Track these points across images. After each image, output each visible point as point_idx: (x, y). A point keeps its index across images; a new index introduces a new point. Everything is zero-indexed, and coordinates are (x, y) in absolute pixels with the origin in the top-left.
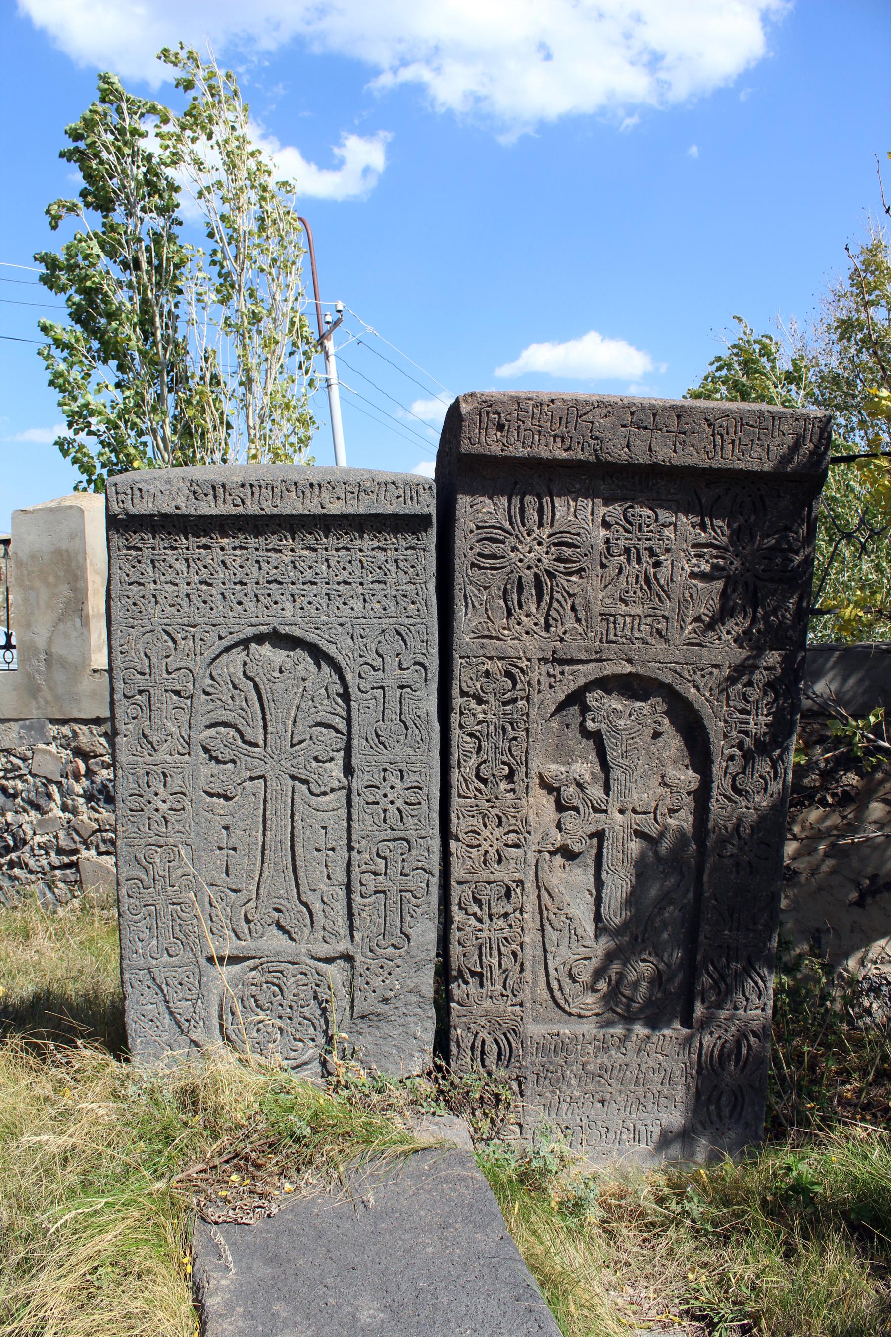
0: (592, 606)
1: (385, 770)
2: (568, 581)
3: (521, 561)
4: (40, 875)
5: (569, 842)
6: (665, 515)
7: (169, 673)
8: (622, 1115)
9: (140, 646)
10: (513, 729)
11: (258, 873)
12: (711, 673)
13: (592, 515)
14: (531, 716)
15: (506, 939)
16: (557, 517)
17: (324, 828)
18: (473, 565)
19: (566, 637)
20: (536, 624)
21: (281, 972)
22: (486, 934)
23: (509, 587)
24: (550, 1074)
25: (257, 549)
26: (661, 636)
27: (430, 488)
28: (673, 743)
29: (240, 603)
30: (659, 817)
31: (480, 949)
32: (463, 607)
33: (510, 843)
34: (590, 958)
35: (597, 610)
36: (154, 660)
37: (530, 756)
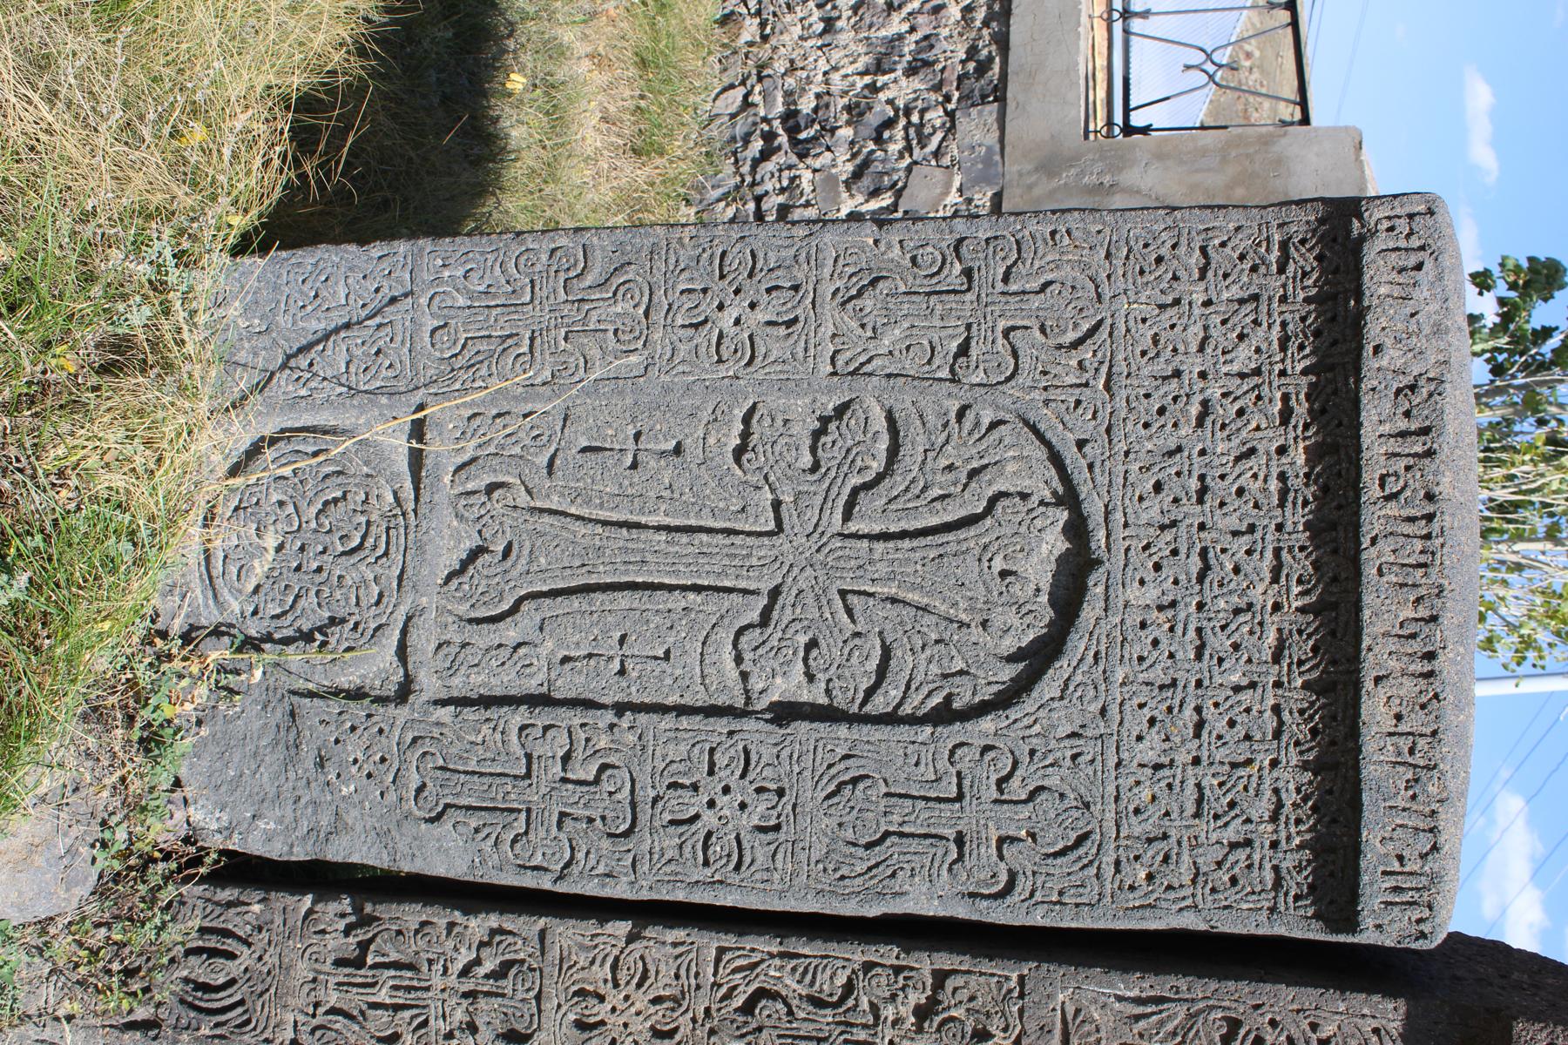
1: (781, 793)
4: (748, 179)
7: (1006, 333)
9: (1067, 273)
11: (585, 512)
15: (425, 1023)
21: (386, 554)
22: (437, 981)
25: (1279, 527)
27: (1423, 935)
29: (1158, 487)
31: (410, 967)
36: (1036, 302)
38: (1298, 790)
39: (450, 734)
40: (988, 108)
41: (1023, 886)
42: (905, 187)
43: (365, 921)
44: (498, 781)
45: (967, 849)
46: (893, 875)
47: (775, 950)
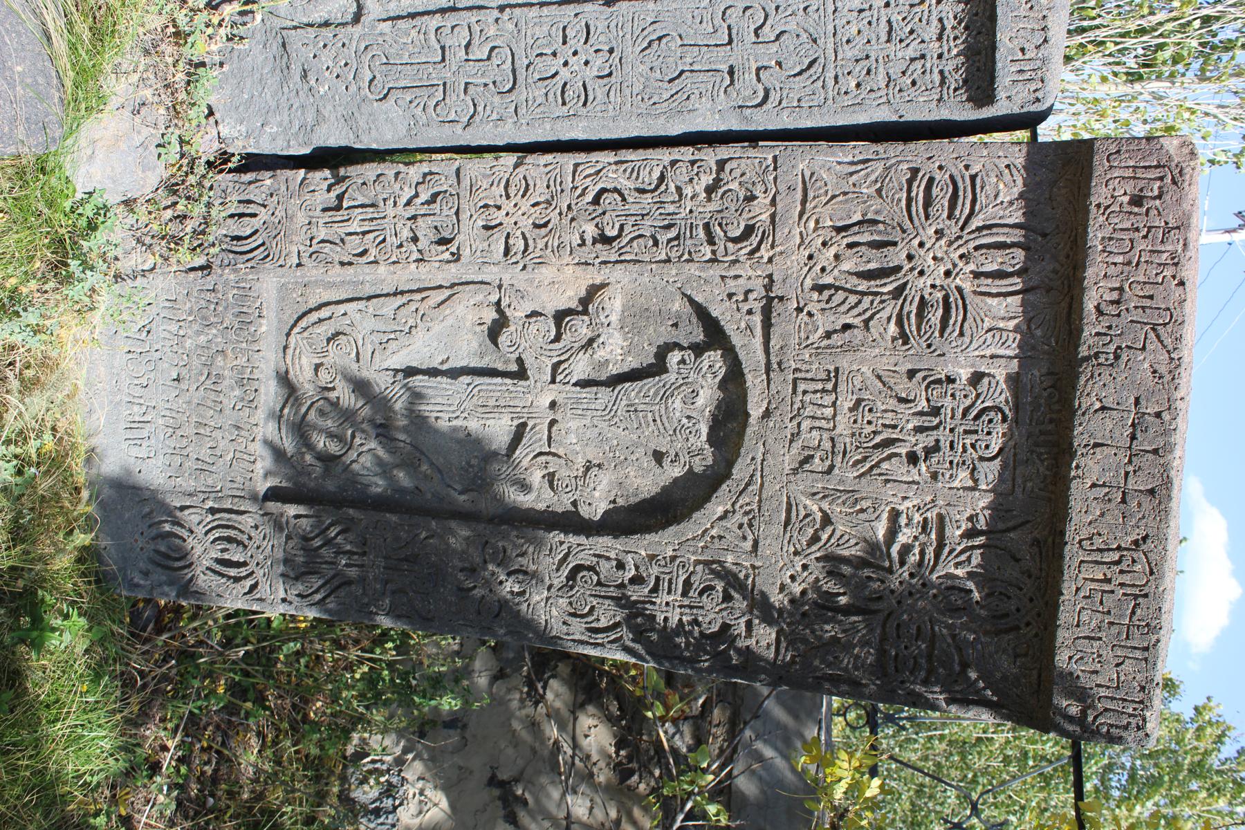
1: (611, 51)
2: (889, 319)
3: (921, 245)
5: (512, 328)
6: (990, 472)
8: (161, 405)
10: (669, 241)
12: (745, 538)
13: (992, 357)
14: (687, 266)
15: (384, 240)
16: (989, 300)
18: (915, 171)
19: (803, 315)
20: (823, 269)
22: (390, 211)
23: (881, 227)
24: (212, 307)
26: (802, 463)
27: (1038, 100)
28: (647, 482)
30: (543, 458)
31: (372, 205)
32: (850, 159)
33: (511, 242)
34: (358, 361)
35: (844, 363)
37: (630, 266)
38: (955, 18)
39: (390, 41)
43: (340, 180)
44: (423, 66)
45: (736, 76)
46: (688, 98)
47: (612, 160)
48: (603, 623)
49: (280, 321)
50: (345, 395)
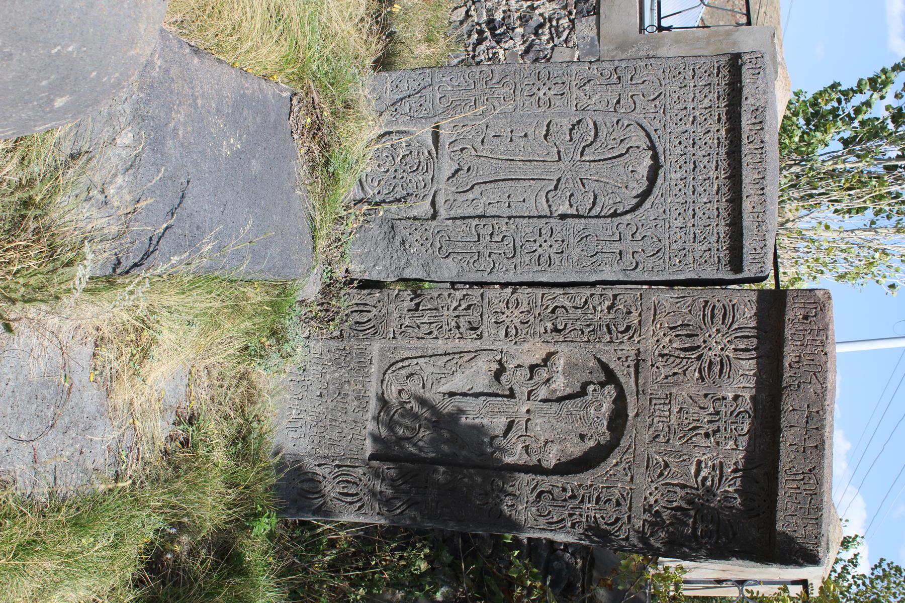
0: (677, 387)
1: (563, 241)
3: (710, 336)
4: (472, 54)
5: (508, 373)
6: (744, 442)
7: (632, 97)
8: (309, 410)
9: (651, 77)
11: (495, 156)
12: (627, 475)
15: (441, 327)
16: (741, 362)
17: (524, 201)
18: (706, 302)
20: (664, 347)
21: (427, 171)
22: (446, 313)
25: (718, 154)
26: (654, 438)
28: (576, 449)
29: (680, 143)
30: (523, 438)
31: (435, 309)
33: (509, 330)
34: (424, 388)
36: (641, 86)
37: (570, 344)
40: (591, 18)
41: (641, 266)
42: (551, 57)
48: (555, 519)
49: (379, 367)
50: (414, 405)
